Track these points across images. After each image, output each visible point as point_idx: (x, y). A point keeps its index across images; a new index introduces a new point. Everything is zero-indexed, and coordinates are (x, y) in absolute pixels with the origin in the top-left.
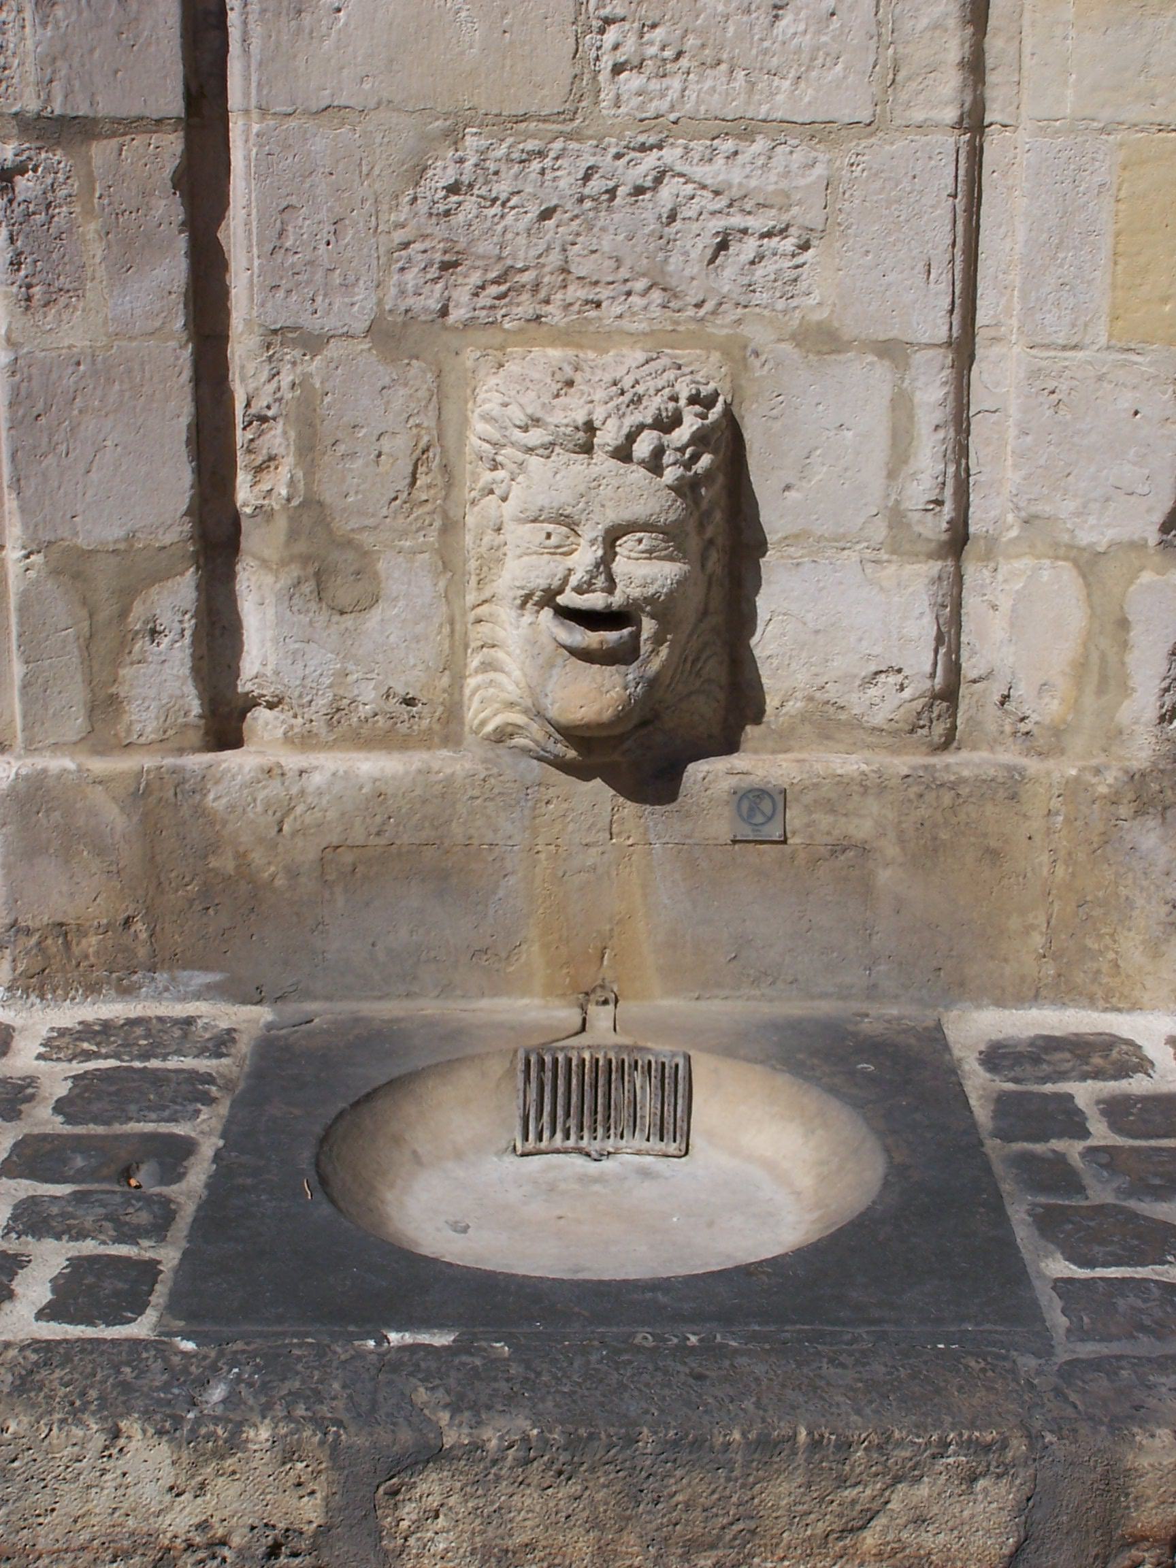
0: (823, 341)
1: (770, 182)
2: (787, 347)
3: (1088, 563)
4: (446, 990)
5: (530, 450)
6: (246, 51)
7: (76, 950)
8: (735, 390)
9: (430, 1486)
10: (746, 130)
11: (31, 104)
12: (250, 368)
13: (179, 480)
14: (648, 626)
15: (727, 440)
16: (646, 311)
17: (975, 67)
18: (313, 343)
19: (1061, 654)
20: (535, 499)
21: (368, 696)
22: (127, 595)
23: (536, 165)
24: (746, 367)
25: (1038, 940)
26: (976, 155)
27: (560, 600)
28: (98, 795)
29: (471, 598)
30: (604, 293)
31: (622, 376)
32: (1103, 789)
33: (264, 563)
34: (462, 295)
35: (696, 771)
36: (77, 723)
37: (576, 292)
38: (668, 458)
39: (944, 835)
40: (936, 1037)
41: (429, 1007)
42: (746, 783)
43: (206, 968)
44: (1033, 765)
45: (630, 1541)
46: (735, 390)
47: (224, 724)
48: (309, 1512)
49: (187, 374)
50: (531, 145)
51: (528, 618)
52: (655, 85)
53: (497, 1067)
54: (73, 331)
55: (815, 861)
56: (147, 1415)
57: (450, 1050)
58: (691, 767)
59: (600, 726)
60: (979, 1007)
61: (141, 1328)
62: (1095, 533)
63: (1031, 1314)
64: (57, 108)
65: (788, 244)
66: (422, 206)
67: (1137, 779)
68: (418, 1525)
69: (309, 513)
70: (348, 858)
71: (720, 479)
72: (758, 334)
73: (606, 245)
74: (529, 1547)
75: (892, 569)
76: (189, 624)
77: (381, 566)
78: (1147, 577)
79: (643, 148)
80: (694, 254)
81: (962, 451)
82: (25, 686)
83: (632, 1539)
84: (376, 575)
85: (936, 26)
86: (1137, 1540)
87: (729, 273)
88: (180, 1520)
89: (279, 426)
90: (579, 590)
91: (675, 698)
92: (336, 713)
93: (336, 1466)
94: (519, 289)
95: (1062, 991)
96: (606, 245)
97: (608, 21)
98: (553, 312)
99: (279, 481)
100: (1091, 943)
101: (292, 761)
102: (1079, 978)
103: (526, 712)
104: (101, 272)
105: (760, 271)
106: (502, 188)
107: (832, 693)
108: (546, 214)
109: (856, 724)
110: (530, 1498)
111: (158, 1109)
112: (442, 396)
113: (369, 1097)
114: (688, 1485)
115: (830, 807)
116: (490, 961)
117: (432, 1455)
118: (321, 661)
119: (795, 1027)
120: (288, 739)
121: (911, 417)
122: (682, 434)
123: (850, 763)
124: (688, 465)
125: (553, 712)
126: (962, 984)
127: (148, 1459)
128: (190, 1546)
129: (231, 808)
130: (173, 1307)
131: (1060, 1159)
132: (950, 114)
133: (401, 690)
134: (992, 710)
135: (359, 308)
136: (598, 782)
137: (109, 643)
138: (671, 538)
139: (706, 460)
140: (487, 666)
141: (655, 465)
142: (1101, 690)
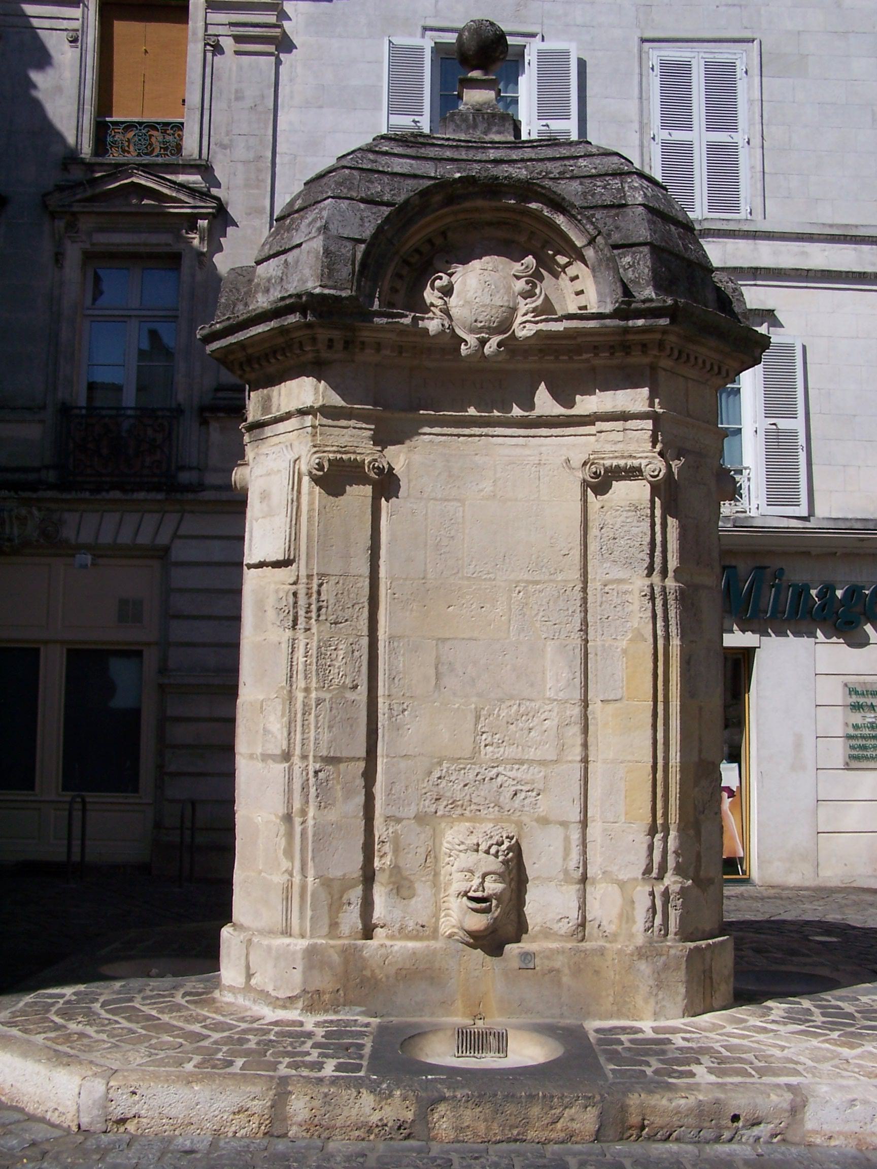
0: (544, 821)
1: (529, 777)
2: (534, 823)
3: (622, 885)
4: (432, 1014)
5: (461, 851)
6: (383, 741)
7: (322, 999)
8: (519, 835)
9: (442, 1108)
10: (522, 762)
11: (324, 753)
12: (380, 827)
13: (359, 858)
14: (494, 902)
15: (517, 849)
16: (494, 813)
17: (585, 745)
18: (399, 820)
19: (615, 911)
20: (461, 865)
21: (411, 925)
22: (342, 893)
23: (463, 772)
24: (522, 828)
25: (611, 999)
26: (586, 769)
27: (469, 894)
28: (332, 951)
29: (442, 896)
30: (481, 807)
31: (487, 831)
32: (629, 952)
33: (382, 884)
34: (441, 807)
35: (508, 947)
36: (325, 930)
37: (473, 807)
38: (500, 854)
39: (582, 966)
40: (581, 1026)
41: (427, 1019)
42: (523, 950)
43: (360, 1006)
44: (608, 945)
45: (495, 1125)
46: (519, 835)
47: (368, 932)
48: (409, 1116)
49: (363, 829)
50: (461, 766)
51: (459, 900)
52: (496, 750)
53: (449, 1033)
54: (332, 815)
55: (544, 975)
56: (367, 1088)
57: (435, 1029)
58: (507, 946)
59: (481, 931)
60: (594, 1020)
61: (362, 1074)
62: (623, 876)
63: (605, 1075)
64: (332, 754)
65: (534, 794)
66: (431, 783)
67: (638, 949)
68: (438, 1120)
69: (396, 869)
70: (404, 972)
71: (515, 861)
72: (525, 819)
73: (482, 794)
74: (468, 1127)
75: (564, 887)
76: (360, 901)
77: (416, 885)
78: (639, 888)
79: (493, 767)
80: (507, 796)
81: (585, 853)
82: (311, 918)
83: (496, 1125)
84: (414, 889)
85: (574, 735)
86: (631, 1127)
87: (517, 802)
88: (375, 1118)
89: (388, 844)
90: (474, 891)
91: (501, 926)
92: (401, 929)
93: (417, 1102)
94: (457, 806)
95: (619, 1015)
96: (482, 794)
97: (483, 733)
98: (467, 813)
99: (387, 860)
100: (627, 999)
101: (388, 943)
102: (624, 1010)
103: (458, 928)
104: (341, 799)
105: (526, 802)
106: (453, 778)
107: (548, 925)
108: (465, 785)
109: (556, 934)
110: (468, 1112)
111: (352, 1037)
112: (435, 836)
113: (413, 1036)
114: (510, 1108)
115: (548, 958)
116: (446, 1005)
117: (443, 1099)
118: (397, 914)
119: (539, 1025)
120: (387, 937)
121: (570, 843)
122: (504, 847)
123: (554, 945)
124: (506, 856)
125: (467, 927)
126: (589, 1013)
127: (368, 1099)
128: (377, 1126)
129: (370, 956)
130: (368, 1070)
131: (617, 1052)
132: (579, 758)
133: (420, 923)
134: (596, 930)
135: (412, 811)
136: (479, 950)
137: (336, 906)
138: (501, 877)
139: (511, 854)
140: (446, 916)
141: (496, 855)
142: (627, 922)
